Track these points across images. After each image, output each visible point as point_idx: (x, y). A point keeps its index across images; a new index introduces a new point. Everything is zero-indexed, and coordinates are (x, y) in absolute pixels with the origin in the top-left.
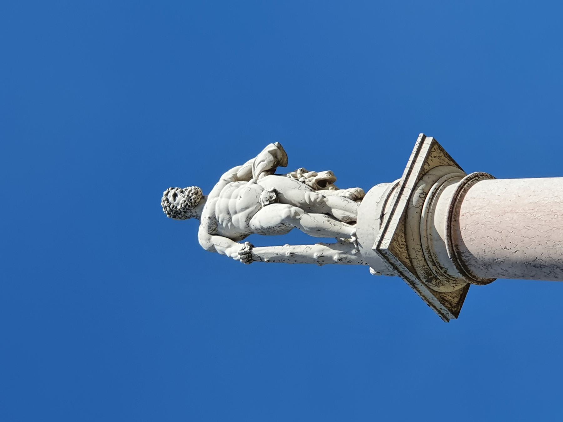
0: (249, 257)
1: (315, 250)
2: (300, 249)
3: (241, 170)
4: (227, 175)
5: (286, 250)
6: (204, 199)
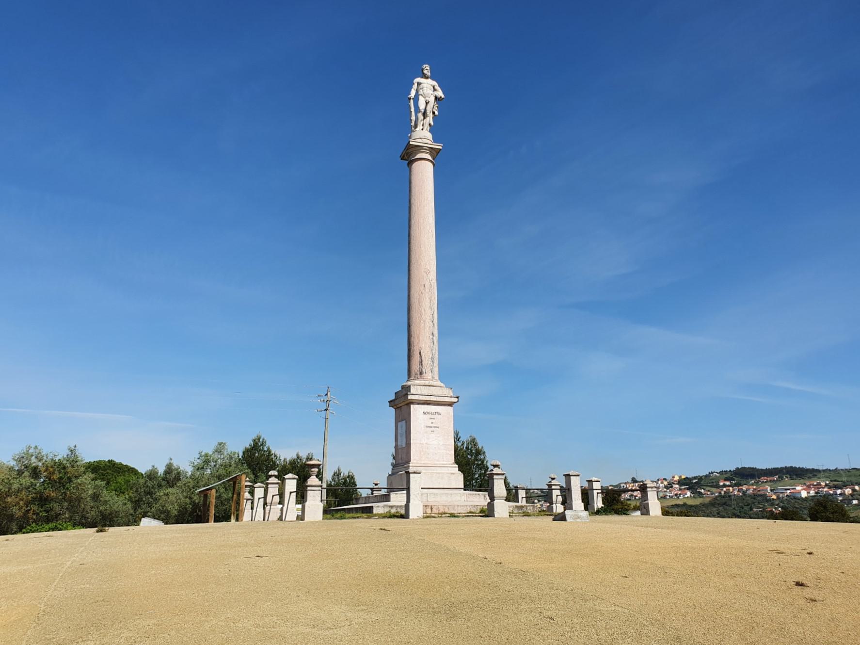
0: (410, 99)
1: (413, 118)
2: (413, 114)
3: (437, 87)
4: (434, 83)
5: (413, 109)
6: (427, 78)
